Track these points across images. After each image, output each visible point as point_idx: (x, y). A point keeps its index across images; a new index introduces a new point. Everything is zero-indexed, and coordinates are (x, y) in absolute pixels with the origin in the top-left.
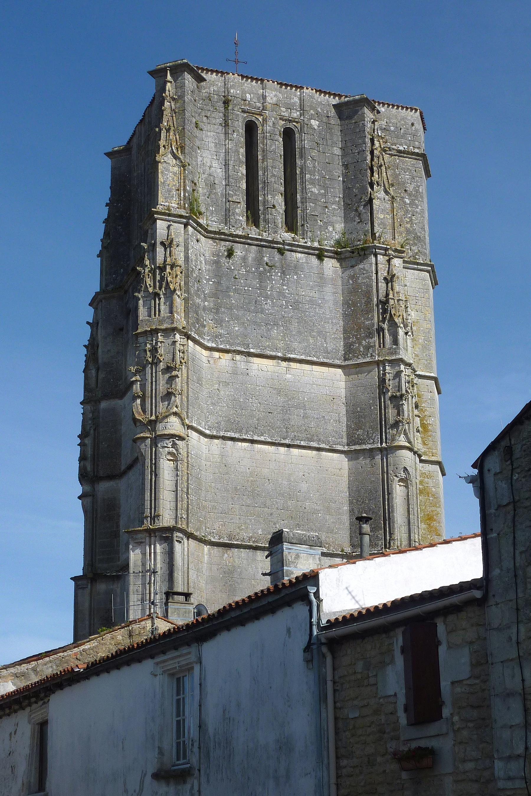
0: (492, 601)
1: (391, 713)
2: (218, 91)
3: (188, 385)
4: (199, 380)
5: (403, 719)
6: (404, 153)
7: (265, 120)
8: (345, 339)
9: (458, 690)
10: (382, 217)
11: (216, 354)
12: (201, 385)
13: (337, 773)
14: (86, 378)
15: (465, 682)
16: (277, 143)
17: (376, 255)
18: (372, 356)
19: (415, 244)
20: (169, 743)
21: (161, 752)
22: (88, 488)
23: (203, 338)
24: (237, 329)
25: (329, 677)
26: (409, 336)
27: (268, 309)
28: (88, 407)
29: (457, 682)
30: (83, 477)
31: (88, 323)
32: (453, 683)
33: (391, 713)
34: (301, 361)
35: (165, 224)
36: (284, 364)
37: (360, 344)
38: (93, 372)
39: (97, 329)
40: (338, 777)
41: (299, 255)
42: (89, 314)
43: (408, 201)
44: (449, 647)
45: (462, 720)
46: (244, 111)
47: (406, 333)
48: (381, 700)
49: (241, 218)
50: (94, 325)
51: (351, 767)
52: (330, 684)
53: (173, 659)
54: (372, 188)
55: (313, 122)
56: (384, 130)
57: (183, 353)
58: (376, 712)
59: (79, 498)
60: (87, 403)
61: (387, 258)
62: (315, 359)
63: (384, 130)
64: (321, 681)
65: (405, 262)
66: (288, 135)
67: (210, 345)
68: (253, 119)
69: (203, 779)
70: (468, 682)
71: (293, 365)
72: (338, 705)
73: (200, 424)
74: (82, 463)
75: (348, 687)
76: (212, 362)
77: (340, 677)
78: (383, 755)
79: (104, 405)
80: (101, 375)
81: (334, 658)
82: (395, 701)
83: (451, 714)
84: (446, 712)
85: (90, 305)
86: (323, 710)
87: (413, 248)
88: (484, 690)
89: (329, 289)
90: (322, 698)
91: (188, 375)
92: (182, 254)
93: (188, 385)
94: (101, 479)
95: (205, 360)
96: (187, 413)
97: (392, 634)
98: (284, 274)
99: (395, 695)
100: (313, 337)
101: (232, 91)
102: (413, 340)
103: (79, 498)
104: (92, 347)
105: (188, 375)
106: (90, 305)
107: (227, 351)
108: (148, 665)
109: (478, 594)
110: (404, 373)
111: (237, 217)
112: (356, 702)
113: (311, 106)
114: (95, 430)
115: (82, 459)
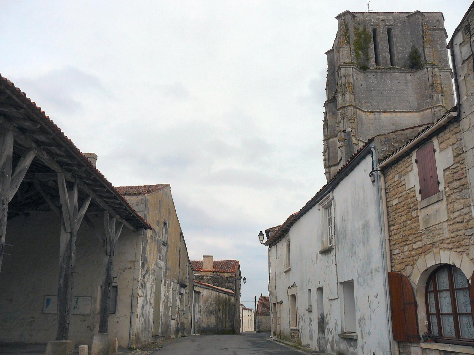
0: (463, 116)
1: (413, 197)
2: (361, 20)
3: (357, 125)
4: (362, 124)
5: (419, 197)
6: (436, 29)
7: (380, 27)
8: (417, 102)
9: (447, 173)
10: (429, 54)
11: (368, 114)
12: (363, 125)
13: (389, 234)
14: (324, 132)
15: (451, 168)
16: (385, 34)
17: (427, 68)
18: (428, 106)
19: (443, 63)
20: (326, 238)
21: (323, 242)
22: (327, 170)
23: (362, 108)
24: (375, 103)
25: (383, 187)
26: (443, 97)
27: (386, 95)
28: (325, 142)
29: (445, 169)
30: (325, 166)
31: (323, 113)
32: (444, 170)
33: (413, 197)
34: (400, 112)
35: (344, 69)
36: (394, 114)
37: (424, 102)
38: (326, 129)
39: (327, 114)
40: (390, 236)
41: (397, 73)
42: (324, 109)
43: (439, 47)
44: (441, 151)
45: (451, 189)
46: (372, 25)
47: (442, 96)
48: (408, 191)
49: (373, 63)
50: (325, 113)
51: (396, 229)
52: (383, 190)
53: (325, 201)
54: (424, 44)
55: (398, 24)
56: (427, 22)
57: (355, 113)
58: (406, 199)
59: (325, 174)
60: (325, 140)
61: (432, 69)
62: (406, 110)
63: (427, 22)
64: (379, 190)
65: (439, 69)
66: (389, 32)
67: (366, 110)
68: (375, 27)
69: (337, 250)
70: (453, 167)
71: (398, 114)
72: (388, 200)
73: (363, 139)
74: (325, 162)
75: (392, 189)
76: (366, 116)
77: (388, 186)
78: (411, 220)
79: (330, 140)
80: (329, 130)
81: (385, 177)
82: (414, 190)
83: (444, 188)
84: (441, 187)
85: (324, 107)
86: (380, 202)
87: (442, 64)
88: (462, 169)
89: (410, 84)
90: (380, 197)
91: (357, 122)
92: (352, 79)
93: (357, 125)
94: (332, 166)
95: (364, 116)
96: (358, 135)
97: (410, 155)
98: (392, 81)
99: (415, 186)
100: (405, 103)
101: (366, 19)
102: (445, 99)
103: (325, 174)
104: (325, 121)
105: (357, 122)
106: (324, 107)
107: (372, 112)
108: (317, 206)
109: (455, 114)
110: (442, 110)
111: (372, 63)
112: (396, 196)
113: (397, 19)
114: (328, 149)
115: (325, 160)
